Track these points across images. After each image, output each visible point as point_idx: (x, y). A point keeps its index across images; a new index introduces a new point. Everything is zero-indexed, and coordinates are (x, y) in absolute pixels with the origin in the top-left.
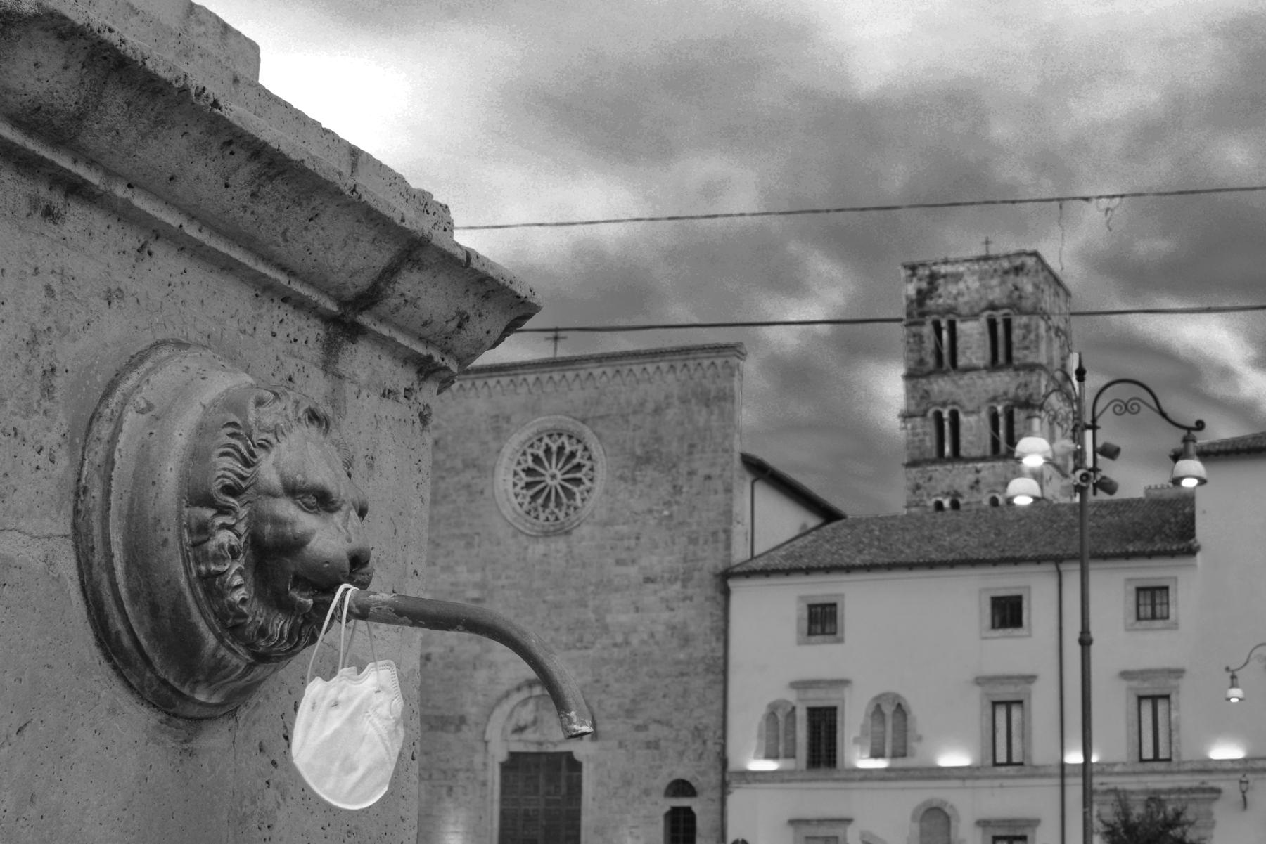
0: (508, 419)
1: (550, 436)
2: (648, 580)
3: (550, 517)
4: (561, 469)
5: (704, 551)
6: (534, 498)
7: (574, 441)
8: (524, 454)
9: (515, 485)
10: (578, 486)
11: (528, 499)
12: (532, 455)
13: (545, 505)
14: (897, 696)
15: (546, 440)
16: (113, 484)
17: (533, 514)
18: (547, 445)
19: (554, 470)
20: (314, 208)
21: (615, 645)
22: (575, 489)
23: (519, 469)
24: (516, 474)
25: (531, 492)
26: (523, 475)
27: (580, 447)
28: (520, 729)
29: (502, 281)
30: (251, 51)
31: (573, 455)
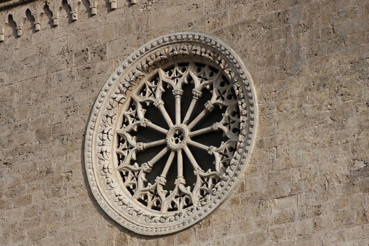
0: (101, 53)
1: (169, 70)
3: (177, 201)
4: (188, 123)
6: (151, 177)
7: (206, 71)
8: (133, 105)
9: (121, 158)
10: (139, 153)
11: (142, 177)
12: (144, 104)
13: (169, 186)
15: (164, 76)
16: (225, 44)
17: (151, 202)
18: (165, 84)
20: (211, 200)
22: (213, 150)
23: (124, 131)
24: (121, 139)
25: (147, 166)
26: (132, 140)
27: (216, 80)
29: (98, 213)
30: (146, 143)
31: (188, 86)
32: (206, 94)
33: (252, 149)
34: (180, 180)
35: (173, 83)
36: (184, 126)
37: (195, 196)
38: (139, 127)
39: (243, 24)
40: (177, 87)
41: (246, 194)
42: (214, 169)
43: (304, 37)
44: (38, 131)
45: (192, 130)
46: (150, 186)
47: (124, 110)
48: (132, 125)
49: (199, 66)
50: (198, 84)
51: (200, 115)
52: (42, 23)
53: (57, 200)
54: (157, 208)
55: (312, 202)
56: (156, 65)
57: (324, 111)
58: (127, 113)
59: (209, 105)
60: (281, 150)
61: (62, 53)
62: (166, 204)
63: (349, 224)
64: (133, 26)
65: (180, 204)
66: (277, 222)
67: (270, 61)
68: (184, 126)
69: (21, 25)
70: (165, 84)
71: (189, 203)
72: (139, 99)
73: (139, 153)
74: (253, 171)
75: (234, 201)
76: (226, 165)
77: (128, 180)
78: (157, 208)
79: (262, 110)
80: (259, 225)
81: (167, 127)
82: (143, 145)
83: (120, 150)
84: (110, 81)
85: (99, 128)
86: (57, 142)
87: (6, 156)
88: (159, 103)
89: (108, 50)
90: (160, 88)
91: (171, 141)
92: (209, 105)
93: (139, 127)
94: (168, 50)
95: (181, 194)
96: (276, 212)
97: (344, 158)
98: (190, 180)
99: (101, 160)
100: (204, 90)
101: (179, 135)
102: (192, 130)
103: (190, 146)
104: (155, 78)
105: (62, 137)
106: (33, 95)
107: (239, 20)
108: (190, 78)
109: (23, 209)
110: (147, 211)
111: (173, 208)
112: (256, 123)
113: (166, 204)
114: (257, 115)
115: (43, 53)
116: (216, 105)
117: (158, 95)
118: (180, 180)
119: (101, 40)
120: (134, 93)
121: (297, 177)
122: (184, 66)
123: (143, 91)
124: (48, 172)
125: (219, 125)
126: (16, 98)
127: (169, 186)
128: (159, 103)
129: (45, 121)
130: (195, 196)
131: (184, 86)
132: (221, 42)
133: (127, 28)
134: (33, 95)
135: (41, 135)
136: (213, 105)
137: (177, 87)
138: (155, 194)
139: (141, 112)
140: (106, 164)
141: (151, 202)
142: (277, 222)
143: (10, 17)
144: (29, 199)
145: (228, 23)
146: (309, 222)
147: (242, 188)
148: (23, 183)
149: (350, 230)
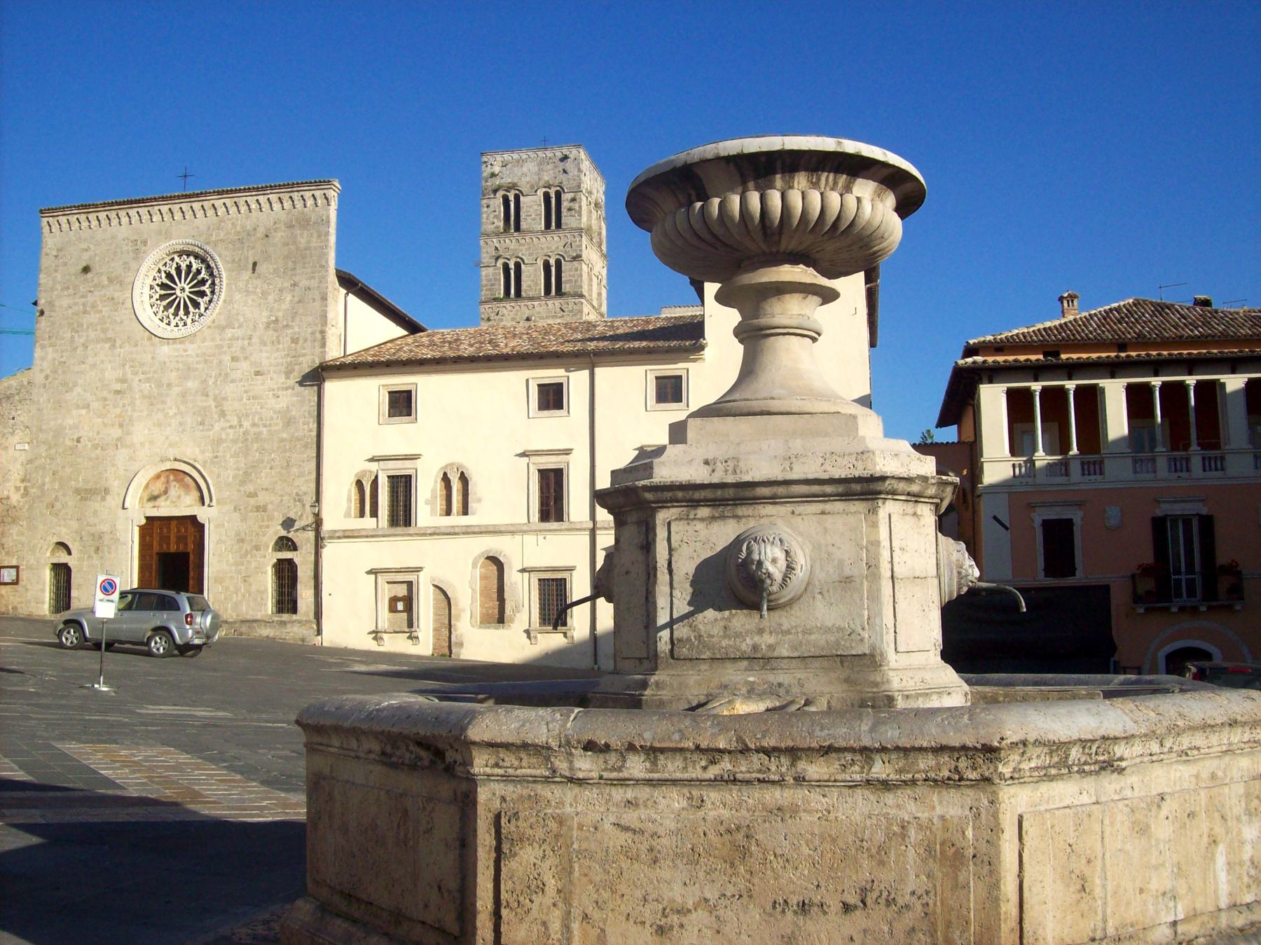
0: (145, 243)
1: (180, 256)
2: (257, 373)
5: (304, 349)
6: (167, 308)
8: (159, 271)
9: (151, 297)
10: (160, 296)
11: (162, 308)
12: (165, 272)
13: (176, 314)
14: (461, 466)
15: (177, 259)
18: (177, 264)
19: (187, 288)
21: (231, 427)
24: (152, 287)
26: (158, 289)
28: (154, 498)
31: (189, 267)
32: (199, 272)
33: (221, 302)
34: (182, 312)
35: (182, 264)
36: (185, 286)
37: (189, 321)
38: (162, 283)
39: (221, 240)
40: (184, 267)
41: (215, 325)
42: (199, 309)
43: (250, 253)
44: (108, 278)
45: (190, 288)
46: (178, 318)
47: (154, 273)
48: (159, 281)
49: (197, 257)
50: (195, 267)
51: (803, 281)
52: (115, 222)
53: (116, 313)
54: (169, 324)
55: (249, 333)
56: (174, 253)
57: (258, 290)
58: (156, 275)
59: (200, 277)
60: (235, 306)
61: (124, 240)
62: (173, 323)
63: (265, 345)
64: (163, 232)
65: (181, 324)
66: (230, 340)
67: (233, 261)
68: (185, 286)
69: (102, 221)
70: (177, 264)
71: (185, 324)
72: (163, 269)
73: (160, 296)
74: (220, 314)
75: (209, 327)
76: (206, 309)
77: (154, 308)
78: (169, 324)
79: (227, 284)
80: (221, 340)
81: (176, 285)
82: (163, 292)
83: (151, 293)
84: (149, 258)
85: (141, 281)
86: (118, 285)
87: (561, 166)
88: (174, 273)
89: (149, 242)
90: (175, 265)
91: (178, 292)
92: (200, 277)
93: (162, 283)
94: (181, 247)
95: (182, 319)
96: (229, 335)
97: (265, 314)
98: (187, 313)
99: (792, 656)
100: (197, 269)
101: (183, 290)
102: (190, 288)
103: (188, 296)
104: (172, 260)
105: (121, 283)
106: (107, 259)
107: (218, 238)
108: (190, 263)
109: (98, 316)
110: (163, 325)
111: (177, 326)
112: (224, 290)
113: (173, 323)
114: (224, 287)
115: (114, 237)
116: (203, 278)
117: (173, 268)
118: (182, 312)
119: (145, 236)
120: (160, 266)
121: (242, 320)
122: (188, 256)
123: (165, 265)
124: (113, 299)
125: (203, 288)
126: (97, 259)
127: (176, 314)
128: (174, 273)
129: (112, 273)
130: (189, 321)
131: (187, 266)
132: (208, 248)
133: (159, 233)
134: (107, 259)
135: (110, 280)
136: (876, 252)
137: (184, 267)
138: (168, 317)
139: (164, 275)
140: (142, 299)
141: (166, 321)
142: (230, 340)
143: (97, 217)
144: (101, 311)
145: (214, 238)
146: (246, 342)
147: (214, 321)
148: (98, 302)
149: (264, 348)
